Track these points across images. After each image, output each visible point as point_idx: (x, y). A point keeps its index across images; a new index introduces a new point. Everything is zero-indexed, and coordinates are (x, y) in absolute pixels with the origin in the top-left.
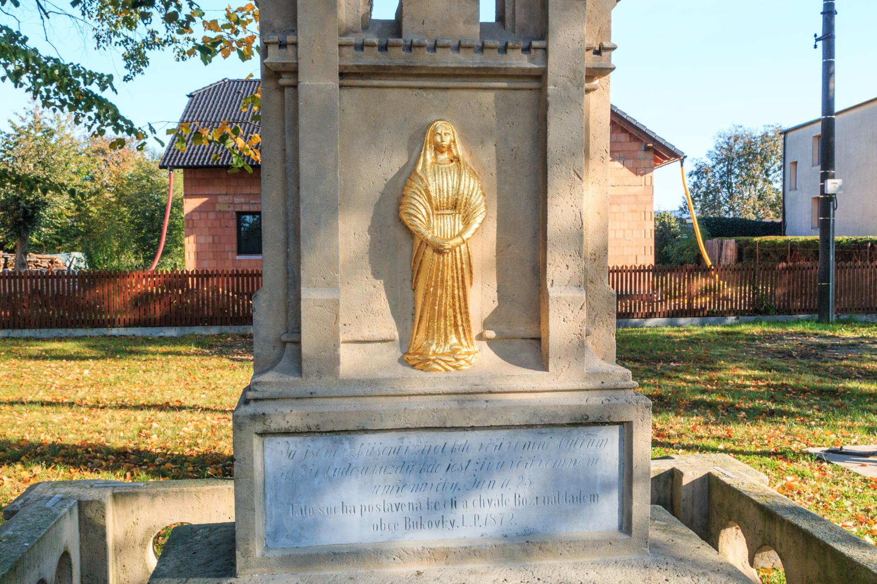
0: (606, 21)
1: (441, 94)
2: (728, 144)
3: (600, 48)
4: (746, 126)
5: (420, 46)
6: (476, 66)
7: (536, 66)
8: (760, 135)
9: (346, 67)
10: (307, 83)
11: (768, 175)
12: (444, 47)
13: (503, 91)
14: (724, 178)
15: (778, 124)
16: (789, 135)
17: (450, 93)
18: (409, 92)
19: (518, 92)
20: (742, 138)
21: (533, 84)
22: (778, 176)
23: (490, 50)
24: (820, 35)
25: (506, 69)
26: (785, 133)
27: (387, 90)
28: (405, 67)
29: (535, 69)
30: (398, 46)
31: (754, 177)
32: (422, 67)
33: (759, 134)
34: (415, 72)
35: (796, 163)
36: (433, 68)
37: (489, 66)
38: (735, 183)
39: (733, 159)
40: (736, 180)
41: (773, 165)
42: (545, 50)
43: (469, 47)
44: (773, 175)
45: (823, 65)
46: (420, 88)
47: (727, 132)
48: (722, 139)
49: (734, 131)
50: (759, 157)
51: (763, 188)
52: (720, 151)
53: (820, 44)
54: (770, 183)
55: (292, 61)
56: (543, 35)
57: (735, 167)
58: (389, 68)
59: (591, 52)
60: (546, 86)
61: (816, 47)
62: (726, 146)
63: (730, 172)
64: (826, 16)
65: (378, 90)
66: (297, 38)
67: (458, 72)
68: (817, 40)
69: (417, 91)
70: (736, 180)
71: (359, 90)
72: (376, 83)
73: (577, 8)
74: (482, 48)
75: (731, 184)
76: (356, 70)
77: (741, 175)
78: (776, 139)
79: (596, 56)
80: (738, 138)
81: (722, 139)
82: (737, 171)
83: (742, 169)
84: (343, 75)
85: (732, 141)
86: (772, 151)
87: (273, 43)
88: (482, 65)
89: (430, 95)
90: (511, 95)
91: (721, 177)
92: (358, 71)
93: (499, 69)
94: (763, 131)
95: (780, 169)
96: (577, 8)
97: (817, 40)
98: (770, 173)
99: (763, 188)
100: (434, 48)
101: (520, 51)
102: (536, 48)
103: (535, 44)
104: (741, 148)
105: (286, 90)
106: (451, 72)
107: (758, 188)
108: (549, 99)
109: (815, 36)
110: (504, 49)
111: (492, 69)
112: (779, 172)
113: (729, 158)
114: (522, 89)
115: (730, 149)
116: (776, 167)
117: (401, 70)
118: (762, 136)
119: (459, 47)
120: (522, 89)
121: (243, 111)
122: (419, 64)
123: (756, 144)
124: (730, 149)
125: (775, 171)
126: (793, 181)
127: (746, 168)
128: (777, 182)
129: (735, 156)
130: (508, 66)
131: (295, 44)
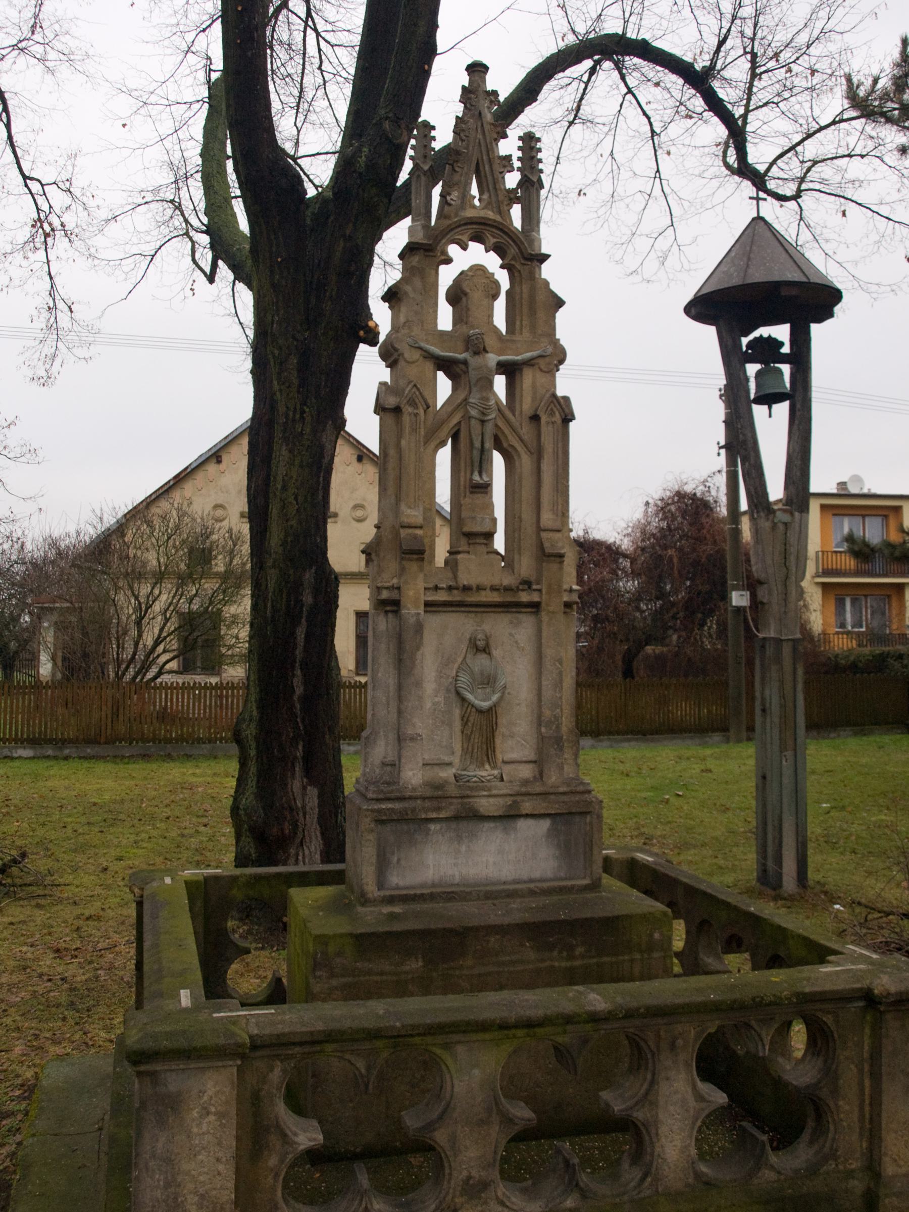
24: (723, 443)
53: (723, 451)
61: (719, 454)
97: (720, 448)
109: (718, 443)
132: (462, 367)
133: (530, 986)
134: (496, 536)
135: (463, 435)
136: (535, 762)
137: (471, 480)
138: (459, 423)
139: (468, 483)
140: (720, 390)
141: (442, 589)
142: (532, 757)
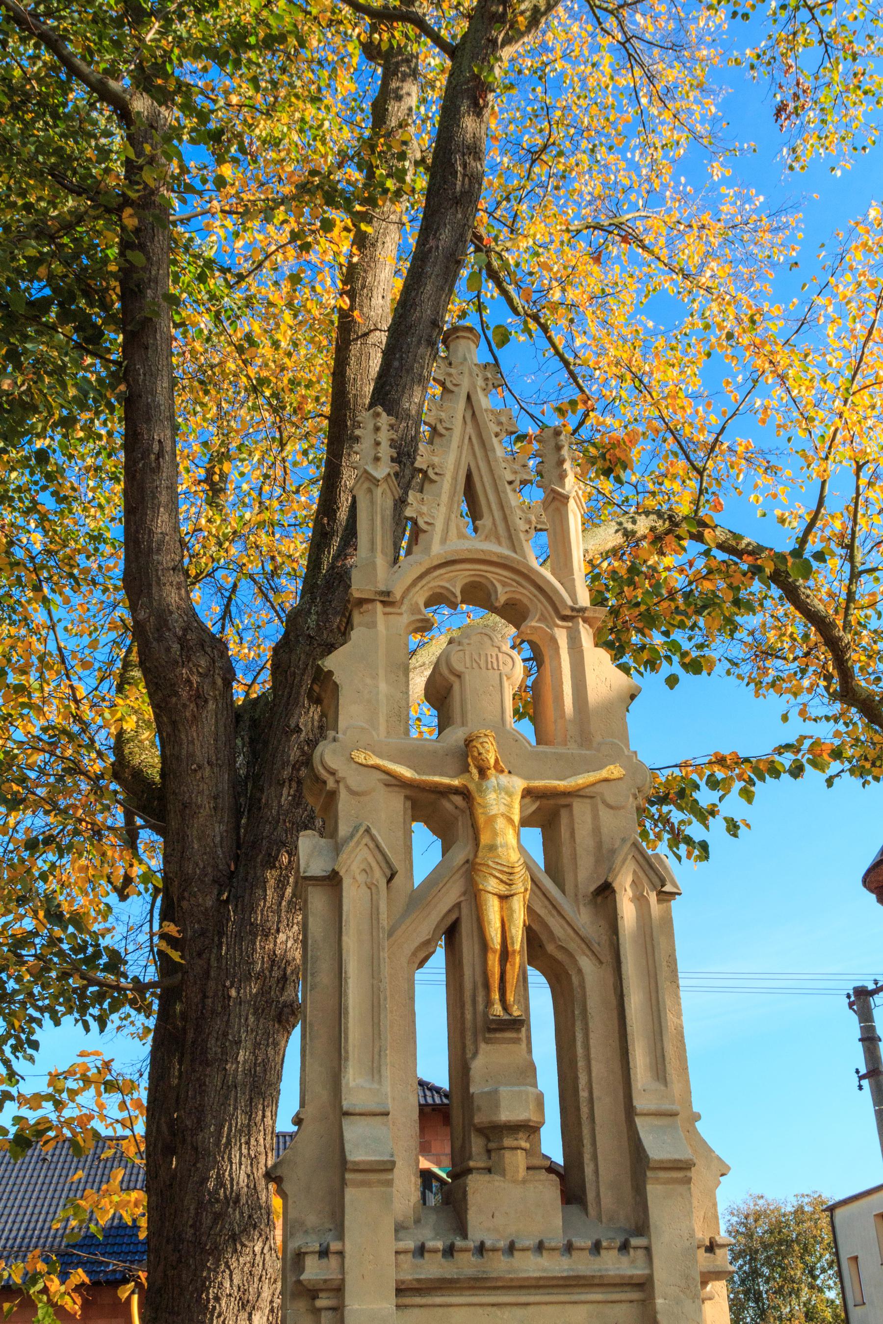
0: (710, 1205)
1: (519, 1312)
2: (745, 1226)
3: (711, 1243)
4: (770, 1196)
5: (494, 1250)
6: (565, 1274)
7: (639, 1272)
8: (792, 1210)
9: (403, 1282)
10: (356, 1307)
11: (815, 1278)
12: (523, 1250)
13: (595, 1305)
14: (749, 1284)
15: (815, 1192)
16: (838, 1212)
17: (531, 1309)
18: (480, 1310)
19: (615, 1305)
20: (767, 1216)
21: (635, 1295)
22: (830, 1278)
23: (579, 1252)
24: (863, 1071)
25: (601, 1277)
26: (832, 1209)
27: (451, 1309)
28: (476, 1279)
29: (637, 1275)
30: (465, 1250)
31: (793, 1282)
32: (496, 1279)
33: (789, 1209)
34: (489, 1285)
35: (856, 1258)
36: (512, 1280)
37: (581, 1274)
38: (766, 1292)
39: (757, 1251)
40: (766, 1287)
41: (819, 1261)
42: (648, 1249)
43: (553, 1249)
44: (822, 1276)
45: (876, 1115)
46: (493, 1305)
47: (742, 1206)
48: (735, 1219)
49: (752, 1207)
50: (796, 1248)
51: (810, 1300)
52: (734, 1237)
53: (865, 1083)
54: (820, 1290)
55: (335, 1276)
56: (642, 1228)
57: (763, 1265)
58: (457, 1281)
59: (703, 1250)
60: (654, 1299)
61: (860, 1088)
62: (742, 1229)
63: (755, 1273)
64: (866, 1043)
65: (440, 1310)
66: (343, 1245)
67: (541, 1283)
68: (861, 1078)
69: (489, 1309)
70: (766, 1287)
71: (416, 1311)
72: (438, 1300)
73: (681, 1194)
74: (569, 1248)
75: (760, 1293)
76: (416, 1285)
77: (774, 1278)
78: (817, 1216)
79: (708, 1255)
80: (760, 1216)
81: (735, 1219)
82: (766, 1271)
83: (772, 1267)
84: (400, 1291)
85: (751, 1220)
86: (815, 1237)
87: (312, 1253)
88: (572, 1273)
89: (506, 1313)
90: (608, 1310)
91: (743, 1282)
92: (417, 1286)
93: (593, 1277)
94: (795, 1204)
95: (831, 1267)
96: (681, 1194)
97: (861, 1078)
98: (817, 1272)
99: (810, 1300)
100: (511, 1249)
101: (616, 1251)
102: (636, 1248)
103: (634, 1242)
104: (766, 1232)
105: (323, 1314)
106: (534, 1283)
107: (804, 1299)
108: (659, 1317)
109: (857, 1071)
110: (597, 1248)
111: (584, 1277)
112: (830, 1272)
113: (750, 1248)
114: (621, 1302)
115: (750, 1236)
116: (824, 1263)
117: (472, 1283)
118: (796, 1212)
119: (540, 1247)
120: (621, 1302)
121: (55, 1227)
122: (494, 1275)
123: (788, 1226)
124: (750, 1236)
125: (823, 1271)
126: (857, 1286)
127: (780, 1266)
128: (830, 1288)
129: (759, 1246)
130: (604, 1273)
131: (341, 1254)
132: (458, 799)
133: (462, 976)
134: (543, 1130)
135: (466, 928)
136: (347, 1114)
137: (486, 1014)
138: (458, 905)
139: (479, 1019)
140: (849, 996)
141: (435, 1251)
142: (347, 1124)
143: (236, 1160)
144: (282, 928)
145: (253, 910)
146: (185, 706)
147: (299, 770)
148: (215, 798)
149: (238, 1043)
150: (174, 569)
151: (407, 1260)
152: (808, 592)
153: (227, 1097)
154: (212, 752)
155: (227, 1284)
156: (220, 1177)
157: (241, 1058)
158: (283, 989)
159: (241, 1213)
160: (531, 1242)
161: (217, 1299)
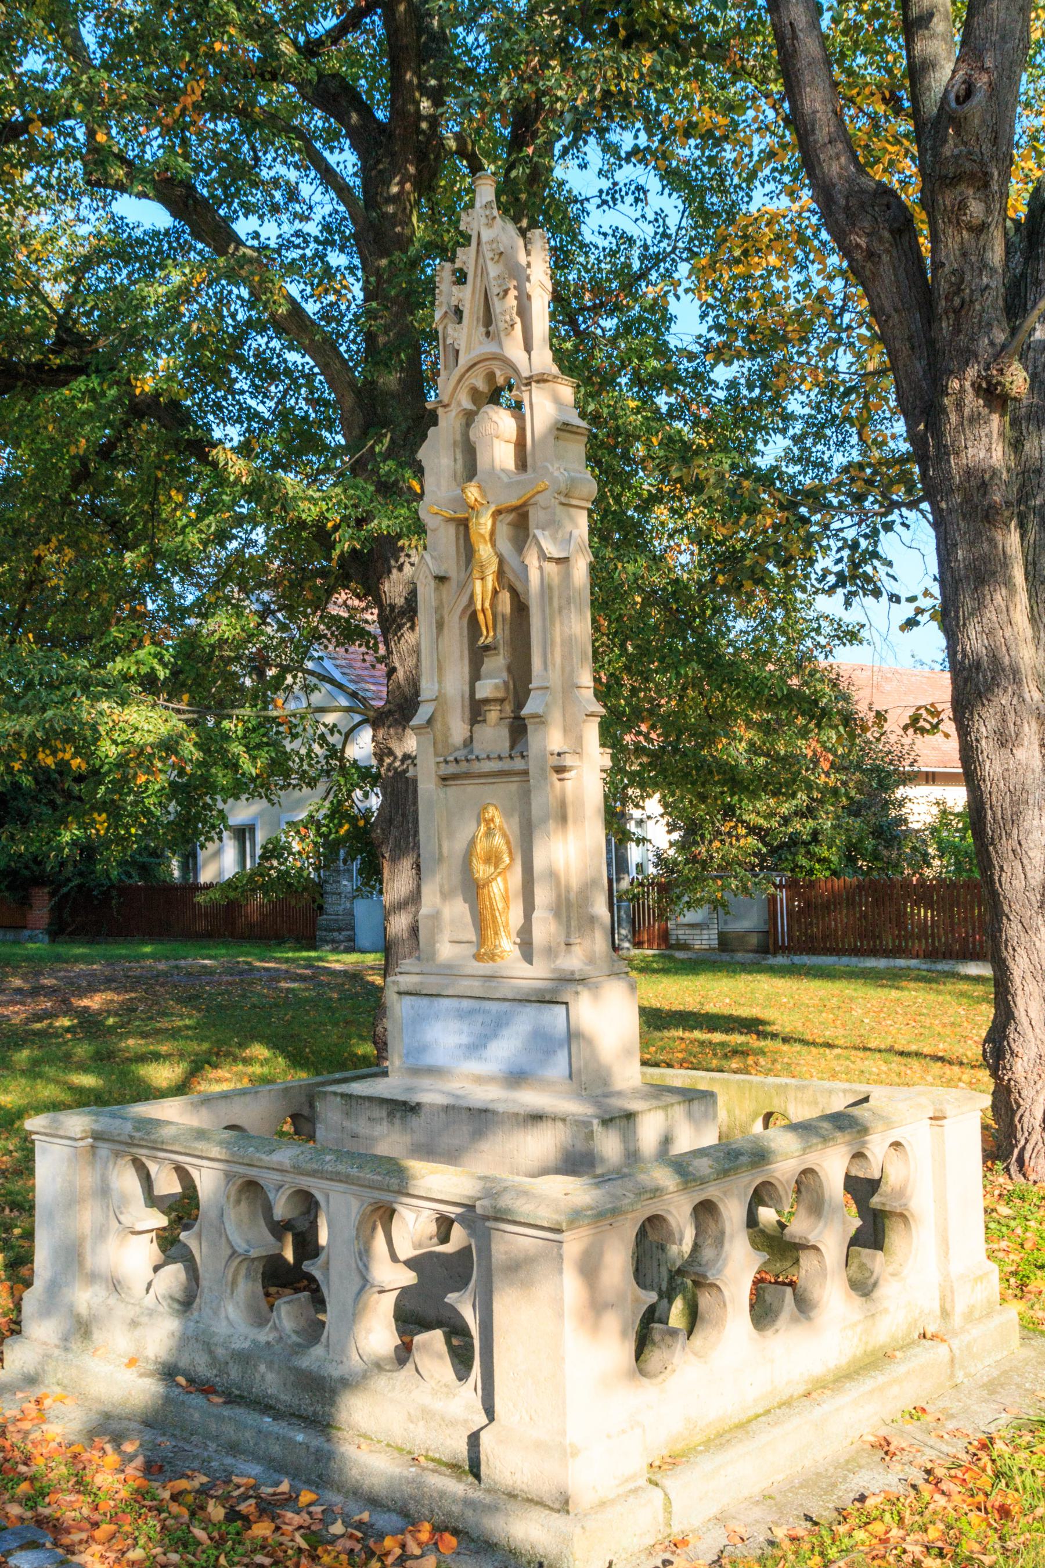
119: (488, 758)
143: (973, 636)
144: (969, 444)
145: (943, 434)
146: (863, 267)
147: (952, 301)
148: (910, 339)
149: (955, 545)
150: (830, 142)
151: (442, 765)
152: (217, 636)
153: (957, 589)
154: (896, 300)
155: (983, 729)
156: (964, 650)
157: (960, 557)
158: (985, 494)
159: (984, 677)
160: (484, 756)
161: (977, 740)
